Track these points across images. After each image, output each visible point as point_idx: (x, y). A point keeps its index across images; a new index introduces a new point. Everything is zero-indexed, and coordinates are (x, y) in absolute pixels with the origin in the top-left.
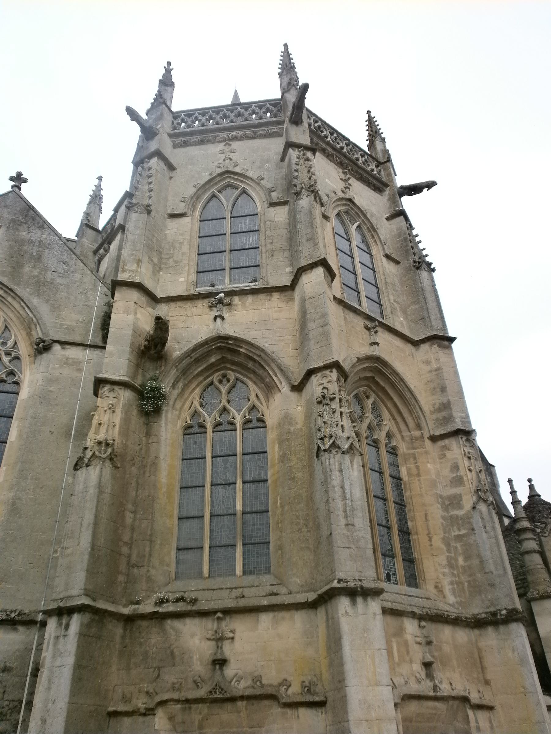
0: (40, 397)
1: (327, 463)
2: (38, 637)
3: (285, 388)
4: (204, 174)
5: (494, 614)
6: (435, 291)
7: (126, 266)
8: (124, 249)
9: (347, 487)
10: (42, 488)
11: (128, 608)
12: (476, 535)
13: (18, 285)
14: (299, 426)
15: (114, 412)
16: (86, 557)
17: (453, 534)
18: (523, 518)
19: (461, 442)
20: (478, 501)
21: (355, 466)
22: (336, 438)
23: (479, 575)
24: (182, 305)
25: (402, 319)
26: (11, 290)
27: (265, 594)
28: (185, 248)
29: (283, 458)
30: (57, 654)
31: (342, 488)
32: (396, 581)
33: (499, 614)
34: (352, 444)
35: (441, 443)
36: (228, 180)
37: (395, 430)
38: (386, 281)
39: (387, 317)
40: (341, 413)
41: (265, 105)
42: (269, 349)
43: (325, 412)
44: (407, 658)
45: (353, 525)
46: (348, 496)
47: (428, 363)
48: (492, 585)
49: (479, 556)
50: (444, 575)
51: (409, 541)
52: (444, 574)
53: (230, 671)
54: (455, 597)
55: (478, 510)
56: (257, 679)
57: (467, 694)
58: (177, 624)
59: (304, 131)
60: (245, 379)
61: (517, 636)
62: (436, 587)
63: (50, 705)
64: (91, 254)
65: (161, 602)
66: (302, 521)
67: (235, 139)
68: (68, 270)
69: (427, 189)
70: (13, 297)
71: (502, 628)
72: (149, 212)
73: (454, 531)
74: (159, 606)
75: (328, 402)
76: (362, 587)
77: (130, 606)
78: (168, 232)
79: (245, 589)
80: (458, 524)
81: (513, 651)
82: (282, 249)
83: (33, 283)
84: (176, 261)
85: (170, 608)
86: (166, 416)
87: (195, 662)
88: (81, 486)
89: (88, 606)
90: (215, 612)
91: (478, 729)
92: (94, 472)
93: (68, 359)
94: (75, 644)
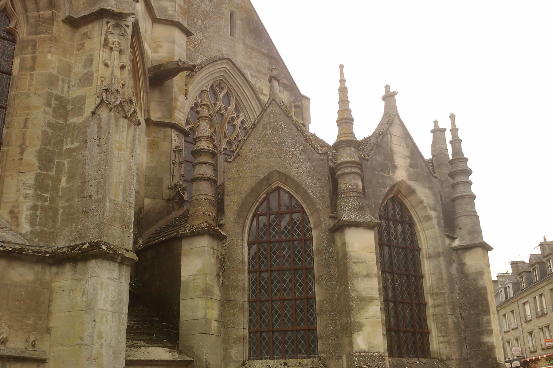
12: (87, 149)
23: (76, 200)
49: (83, 176)
52: (26, 196)
55: (98, 117)
61: (92, 277)
62: (11, 212)
71: (80, 266)
73: (67, 144)
80: (73, 134)
81: (83, 294)
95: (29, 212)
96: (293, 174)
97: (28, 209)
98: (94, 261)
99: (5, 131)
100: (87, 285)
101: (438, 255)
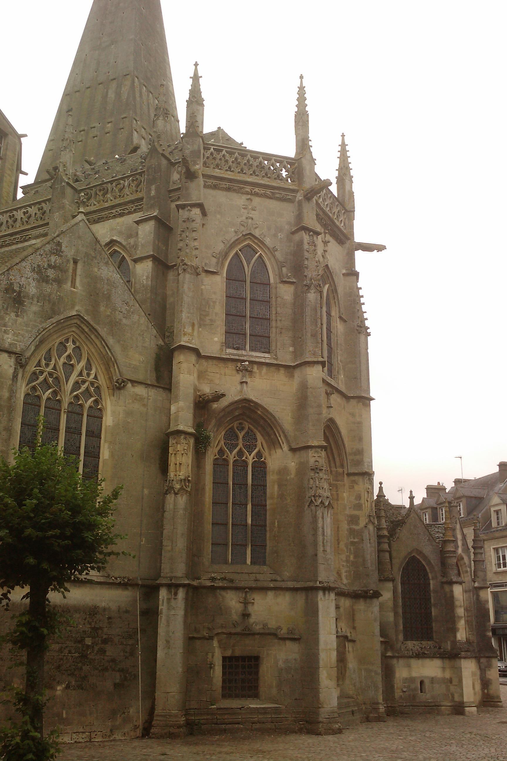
3: (285, 448)
5: (366, 592)
6: (367, 353)
9: (325, 528)
13: (98, 324)
14: (292, 476)
16: (184, 555)
17: (350, 540)
18: (385, 528)
24: (217, 363)
27: (270, 580)
29: (281, 496)
35: (352, 478)
42: (277, 415)
46: (325, 534)
48: (367, 575)
53: (252, 620)
56: (265, 625)
58: (223, 593)
60: (255, 430)
62: (338, 573)
65: (213, 579)
67: (257, 195)
70: (95, 335)
71: (368, 600)
75: (318, 471)
76: (330, 586)
78: (203, 287)
81: (372, 613)
84: (211, 320)
88: (171, 506)
90: (245, 588)
92: (182, 499)
93: (137, 395)
94: (184, 604)
95: (346, 574)
96: (424, 552)
97: (345, 572)
101: (470, 591)
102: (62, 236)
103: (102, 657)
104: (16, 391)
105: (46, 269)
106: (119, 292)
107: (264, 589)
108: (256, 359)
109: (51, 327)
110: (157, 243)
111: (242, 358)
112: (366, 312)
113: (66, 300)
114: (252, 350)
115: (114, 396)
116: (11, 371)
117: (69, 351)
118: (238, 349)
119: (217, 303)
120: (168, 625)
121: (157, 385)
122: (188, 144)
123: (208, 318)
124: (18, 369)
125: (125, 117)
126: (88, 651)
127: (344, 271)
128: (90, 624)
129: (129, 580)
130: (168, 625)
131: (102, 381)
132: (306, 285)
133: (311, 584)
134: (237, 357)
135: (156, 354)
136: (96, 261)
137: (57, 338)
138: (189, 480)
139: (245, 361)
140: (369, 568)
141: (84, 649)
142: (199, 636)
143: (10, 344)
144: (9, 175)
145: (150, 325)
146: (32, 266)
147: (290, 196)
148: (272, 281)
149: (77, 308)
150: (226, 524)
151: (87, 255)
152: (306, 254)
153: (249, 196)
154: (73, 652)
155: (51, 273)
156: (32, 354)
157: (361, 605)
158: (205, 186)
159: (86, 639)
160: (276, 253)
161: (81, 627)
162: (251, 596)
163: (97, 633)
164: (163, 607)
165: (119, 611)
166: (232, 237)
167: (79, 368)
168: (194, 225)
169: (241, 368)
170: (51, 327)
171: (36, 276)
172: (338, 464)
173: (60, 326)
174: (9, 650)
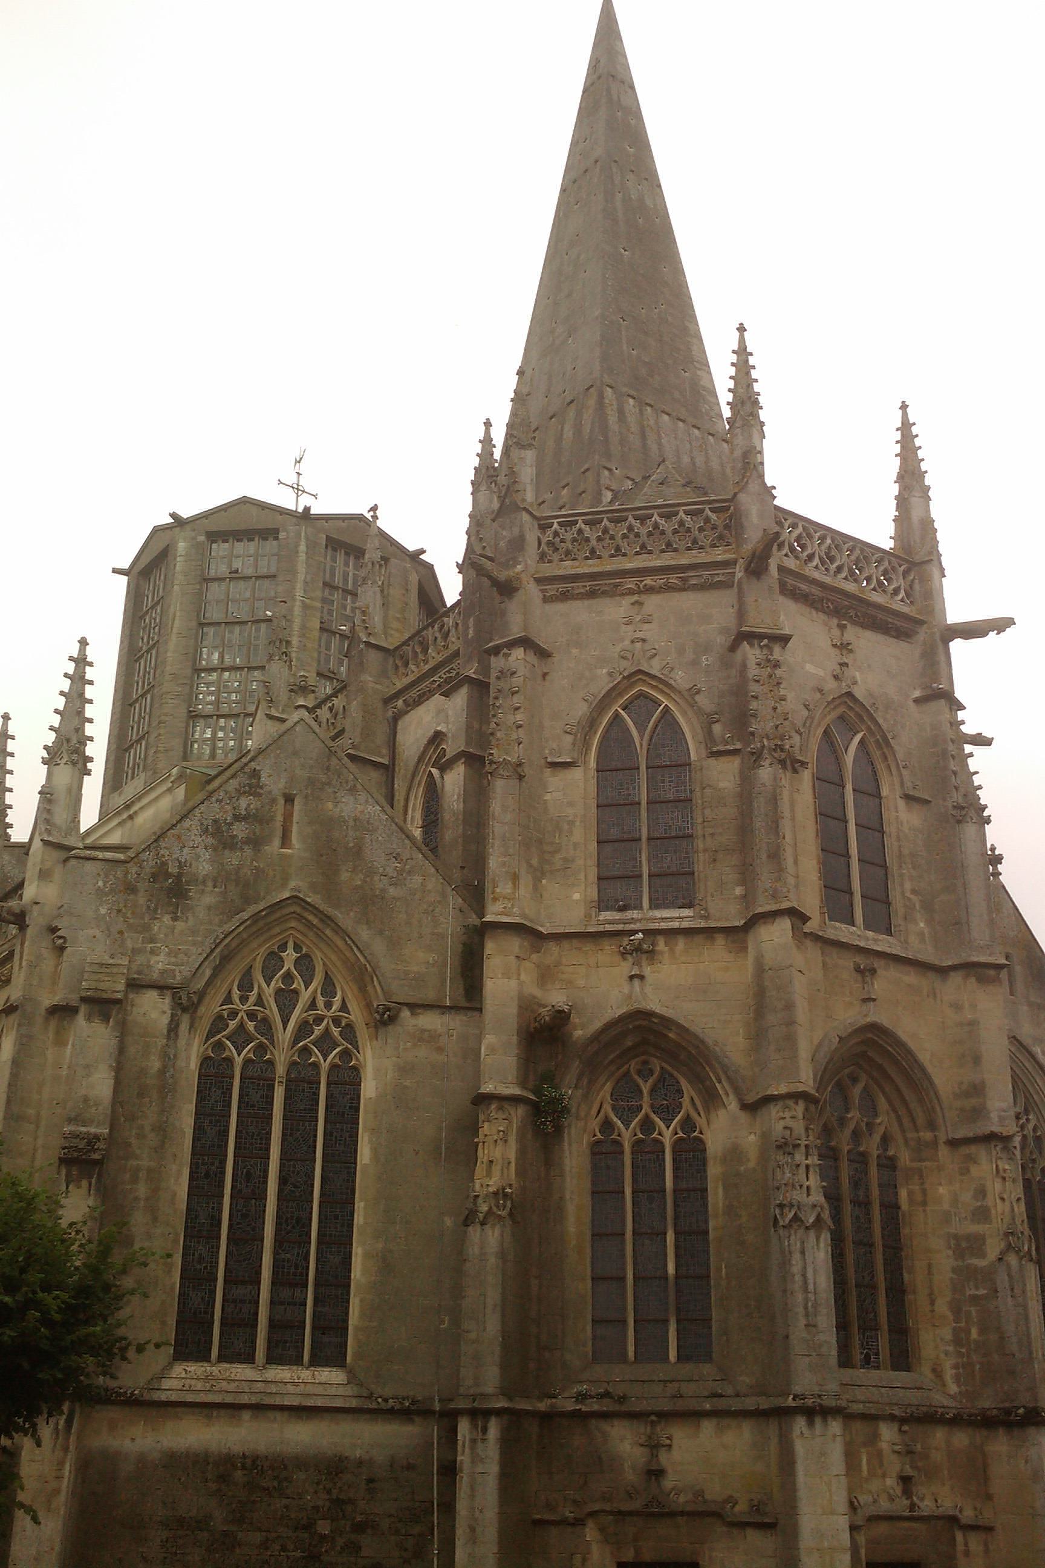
0: (394, 1098)
1: (786, 1244)
2: (438, 1428)
3: (733, 1105)
4: (599, 671)
5: (1008, 1412)
7: (497, 887)
8: (491, 857)
9: (810, 1275)
10: (414, 1234)
11: (544, 1404)
14: (752, 1164)
15: (506, 1141)
16: (498, 1350)
19: (994, 1153)
20: (1008, 1250)
21: (822, 1245)
22: (799, 1208)
23: (996, 1357)
25: (922, 925)
26: (329, 918)
27: (706, 1394)
28: (578, 835)
29: (730, 1210)
30: (476, 1459)
31: (804, 1276)
32: (878, 1363)
33: (1013, 1414)
34: (819, 1215)
35: (964, 1150)
36: (640, 677)
37: (895, 1129)
38: (900, 851)
39: (897, 929)
40: (807, 1167)
41: (702, 511)
43: (785, 1166)
44: (880, 1472)
45: (815, 1326)
46: (811, 1287)
47: (957, 1007)
50: (946, 1355)
51: (903, 1301)
52: (947, 1353)
53: (668, 1483)
54: (959, 1386)
56: (700, 1493)
57: (958, 1513)
58: (605, 1426)
59: (770, 588)
62: (934, 1370)
63: (477, 1513)
64: (380, 705)
65: (581, 1397)
66: (753, 1303)
67: (650, 590)
68: (403, 870)
69: (996, 632)
70: (333, 930)
72: (521, 778)
74: (582, 1403)
76: (821, 1405)
77: (546, 1400)
78: (548, 797)
79: (682, 1383)
81: (1026, 1462)
82: (728, 848)
83: (357, 902)
84: (565, 860)
85: (595, 1406)
86: (569, 1134)
87: (627, 1470)
88: (476, 1251)
89: (507, 1409)
91: (967, 1553)
92: (493, 1232)
93: (423, 1031)
94: (498, 1452)
97: (951, 1368)
98: (1033, 1428)
99: (906, 1275)
100: (1029, 1453)
102: (260, 758)
103: (352, 1559)
104: (175, 1056)
105: (231, 824)
106: (380, 838)
107: (695, 1416)
108: (663, 924)
109: (242, 928)
110: (476, 725)
111: (632, 927)
112: (977, 773)
113: (271, 873)
114: (655, 905)
115: (377, 1039)
116: (165, 1020)
117: (289, 965)
118: (623, 909)
119: (578, 823)
120: (472, 1497)
121: (468, 1005)
122: (503, 529)
123: (558, 856)
124: (177, 1015)
125: (588, 470)
126: (322, 1547)
127: (917, 694)
128: (329, 1492)
129: (413, 1403)
130: (472, 1497)
131: (357, 1015)
132: (753, 754)
133: (779, 1402)
134: (620, 927)
135: (464, 944)
136: (330, 790)
137: (260, 946)
138: (505, 1195)
139: (636, 932)
140: (1014, 1355)
141: (313, 1543)
142: (553, 1518)
143: (163, 972)
144: (397, 630)
145: (449, 889)
146: (202, 824)
147: (720, 575)
148: (693, 756)
149: (292, 884)
150: (623, 1279)
151: (311, 782)
152: (754, 688)
153: (636, 597)
154: (291, 1547)
155: (240, 830)
156: (209, 983)
157: (1000, 1445)
158: (546, 600)
159: (320, 1522)
160: (697, 698)
161: (309, 1497)
162: (664, 1431)
163: (342, 1510)
164: (464, 1458)
165: (391, 1466)
166: (602, 684)
167: (305, 996)
168: (516, 681)
169: (628, 947)
170: (242, 928)
171: (210, 840)
172: (921, 1120)
173: (261, 923)
174: (161, 1542)
